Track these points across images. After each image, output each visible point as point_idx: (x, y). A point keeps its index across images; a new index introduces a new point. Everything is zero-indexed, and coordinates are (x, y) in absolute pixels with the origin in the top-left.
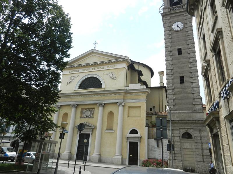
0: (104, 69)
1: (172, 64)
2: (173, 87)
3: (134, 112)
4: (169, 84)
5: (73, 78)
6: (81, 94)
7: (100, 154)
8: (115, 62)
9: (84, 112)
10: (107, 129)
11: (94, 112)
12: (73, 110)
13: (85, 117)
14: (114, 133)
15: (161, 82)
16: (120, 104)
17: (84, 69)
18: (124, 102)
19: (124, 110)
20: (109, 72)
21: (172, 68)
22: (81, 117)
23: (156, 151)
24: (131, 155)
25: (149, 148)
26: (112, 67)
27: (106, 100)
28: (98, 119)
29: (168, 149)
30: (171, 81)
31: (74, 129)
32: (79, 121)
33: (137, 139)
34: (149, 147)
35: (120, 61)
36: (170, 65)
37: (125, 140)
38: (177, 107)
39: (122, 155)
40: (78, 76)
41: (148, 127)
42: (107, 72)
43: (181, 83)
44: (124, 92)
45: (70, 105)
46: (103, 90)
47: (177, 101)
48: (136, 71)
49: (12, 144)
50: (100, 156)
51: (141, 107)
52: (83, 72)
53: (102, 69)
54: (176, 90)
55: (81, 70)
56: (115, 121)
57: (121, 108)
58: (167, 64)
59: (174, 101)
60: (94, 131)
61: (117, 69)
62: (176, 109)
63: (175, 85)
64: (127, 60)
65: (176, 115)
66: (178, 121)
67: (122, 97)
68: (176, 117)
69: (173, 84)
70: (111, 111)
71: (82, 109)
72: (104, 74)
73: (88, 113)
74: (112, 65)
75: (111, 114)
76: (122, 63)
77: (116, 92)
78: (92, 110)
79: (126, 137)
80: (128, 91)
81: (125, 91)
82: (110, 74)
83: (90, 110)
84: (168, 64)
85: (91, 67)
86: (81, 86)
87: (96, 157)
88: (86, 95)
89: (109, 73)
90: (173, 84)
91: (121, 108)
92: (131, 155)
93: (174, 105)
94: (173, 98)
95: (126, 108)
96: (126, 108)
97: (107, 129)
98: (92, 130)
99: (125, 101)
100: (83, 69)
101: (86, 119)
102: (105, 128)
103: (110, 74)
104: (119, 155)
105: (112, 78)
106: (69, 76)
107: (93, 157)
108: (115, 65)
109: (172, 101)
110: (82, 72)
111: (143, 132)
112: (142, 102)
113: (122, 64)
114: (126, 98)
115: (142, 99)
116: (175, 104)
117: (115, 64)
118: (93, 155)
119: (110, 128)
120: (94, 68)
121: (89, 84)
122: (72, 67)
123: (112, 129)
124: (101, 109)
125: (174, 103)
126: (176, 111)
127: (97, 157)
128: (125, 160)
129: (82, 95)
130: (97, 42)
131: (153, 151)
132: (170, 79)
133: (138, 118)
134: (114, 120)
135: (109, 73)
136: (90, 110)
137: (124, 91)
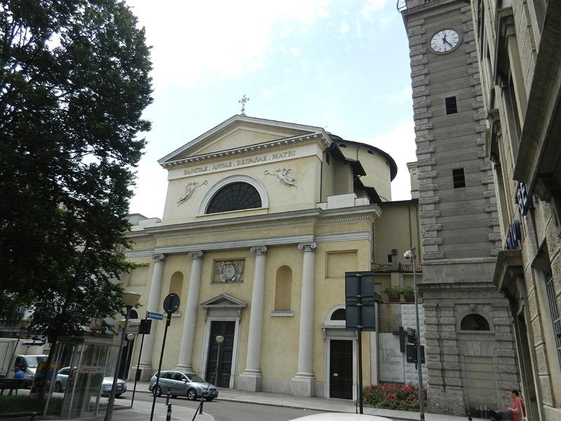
0: (265, 162)
1: (431, 138)
2: (437, 199)
5: (193, 187)
7: (260, 372)
10: (276, 310)
11: (243, 269)
12: (195, 263)
13: (224, 281)
15: (415, 189)
18: (315, 240)
19: (315, 263)
21: (431, 150)
22: (213, 282)
23: (397, 363)
24: (336, 375)
25: (381, 356)
26: (284, 155)
27: (271, 238)
31: (197, 310)
34: (381, 352)
35: (304, 139)
36: (428, 143)
37: (320, 336)
38: (446, 248)
40: (205, 183)
42: (272, 169)
46: (265, 212)
47: (446, 234)
51: (358, 252)
52: (217, 171)
53: (261, 163)
54: (443, 206)
55: (210, 168)
56: (294, 289)
59: (440, 233)
61: (297, 161)
64: (319, 136)
65: (445, 269)
67: (311, 229)
68: (444, 274)
69: (437, 190)
70: (290, 266)
71: (216, 261)
72: (267, 173)
73: (230, 272)
75: (285, 271)
76: (309, 144)
77: (296, 218)
80: (324, 214)
81: (318, 214)
90: (437, 190)
91: (308, 256)
92: (336, 375)
94: (436, 227)
95: (322, 257)
96: (322, 257)
97: (276, 310)
98: (240, 311)
102: (271, 306)
104: (252, 370)
105: (286, 184)
106: (185, 183)
107: (243, 378)
109: (435, 233)
110: (214, 171)
111: (62, 38)
113: (307, 147)
114: (319, 231)
115: (360, 232)
118: (242, 373)
119: (283, 307)
120: (241, 159)
122: (189, 161)
123: (287, 310)
124: (259, 260)
127: (253, 378)
128: (322, 387)
132: (428, 178)
134: (293, 285)
135: (278, 171)
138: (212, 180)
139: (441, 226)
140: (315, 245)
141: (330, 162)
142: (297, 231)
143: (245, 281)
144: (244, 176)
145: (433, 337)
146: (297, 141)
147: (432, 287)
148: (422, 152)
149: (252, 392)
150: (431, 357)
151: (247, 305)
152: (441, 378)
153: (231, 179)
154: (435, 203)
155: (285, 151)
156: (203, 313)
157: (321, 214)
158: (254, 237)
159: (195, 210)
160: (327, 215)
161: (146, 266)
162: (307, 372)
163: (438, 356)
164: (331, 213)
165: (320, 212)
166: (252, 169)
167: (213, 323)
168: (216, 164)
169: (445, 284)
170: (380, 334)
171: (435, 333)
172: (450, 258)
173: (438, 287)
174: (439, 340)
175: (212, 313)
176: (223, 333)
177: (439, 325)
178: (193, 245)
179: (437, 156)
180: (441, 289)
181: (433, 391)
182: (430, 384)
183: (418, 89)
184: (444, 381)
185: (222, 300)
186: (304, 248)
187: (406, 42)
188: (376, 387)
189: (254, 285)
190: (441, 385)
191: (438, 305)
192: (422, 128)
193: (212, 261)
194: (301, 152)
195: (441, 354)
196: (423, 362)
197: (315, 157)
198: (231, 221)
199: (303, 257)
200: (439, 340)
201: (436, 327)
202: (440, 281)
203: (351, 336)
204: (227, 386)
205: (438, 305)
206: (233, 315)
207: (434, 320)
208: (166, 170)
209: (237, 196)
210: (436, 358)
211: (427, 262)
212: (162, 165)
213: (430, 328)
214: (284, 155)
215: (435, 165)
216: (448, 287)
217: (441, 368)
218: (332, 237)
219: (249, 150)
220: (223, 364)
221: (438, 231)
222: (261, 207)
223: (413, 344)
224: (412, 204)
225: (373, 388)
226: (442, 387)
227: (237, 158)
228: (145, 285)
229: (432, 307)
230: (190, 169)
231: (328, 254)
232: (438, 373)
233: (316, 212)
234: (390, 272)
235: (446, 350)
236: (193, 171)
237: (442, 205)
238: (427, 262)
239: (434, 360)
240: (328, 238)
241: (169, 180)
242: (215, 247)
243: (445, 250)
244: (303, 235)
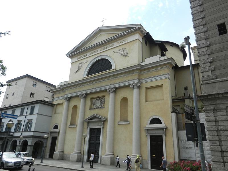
1: (201, 10)
2: (208, 43)
3: (154, 94)
4: (200, 40)
5: (81, 64)
7: (113, 154)
8: (125, 35)
10: (120, 121)
11: (104, 101)
12: (82, 100)
13: (95, 108)
14: (129, 125)
15: (196, 59)
16: (134, 85)
18: (139, 82)
19: (140, 94)
20: (119, 49)
21: (202, 16)
22: (91, 109)
23: (191, 148)
24: (154, 155)
25: (180, 144)
26: (122, 42)
28: (109, 109)
29: (190, 136)
30: (203, 35)
31: (83, 123)
32: (89, 114)
33: (161, 131)
34: (179, 141)
35: (132, 32)
36: (200, 13)
37: (144, 134)
38: (217, 72)
39: (141, 154)
41: (176, 112)
42: (116, 50)
43: (220, 35)
44: (138, 69)
46: (114, 70)
47: (216, 64)
48: (156, 45)
49: (23, 144)
50: (112, 157)
51: (163, 86)
52: (92, 55)
54: (213, 47)
55: (88, 54)
56: (129, 109)
57: (136, 91)
58: (194, 13)
59: (212, 64)
60: (106, 123)
61: (129, 44)
62: (216, 76)
63: (210, 40)
64: (139, 28)
65: (217, 85)
66: (222, 94)
67: (137, 77)
68: (217, 88)
69: (208, 39)
70: (124, 97)
71: (92, 99)
73: (98, 103)
75: (125, 100)
76: (134, 34)
77: (128, 71)
78: (102, 99)
79: (145, 129)
80: (143, 67)
81: (139, 67)
82: (120, 52)
83: (101, 99)
84: (196, 12)
85: (99, 48)
86: (90, 72)
87: (108, 158)
90: (208, 39)
91: (136, 91)
92: (154, 155)
93: (212, 71)
94: (209, 60)
95: (144, 91)
96: (144, 91)
97: (120, 121)
98: (102, 122)
99: (140, 81)
101: (97, 110)
102: (118, 119)
103: (120, 52)
104: (112, 154)
105: (123, 56)
106: (78, 63)
107: (104, 157)
108: (126, 39)
109: (208, 64)
110: (90, 55)
111: (169, 120)
112: (165, 79)
113: (133, 35)
114: (142, 77)
115: (163, 75)
116: (214, 68)
117: (125, 38)
118: (104, 155)
119: (124, 119)
120: (102, 48)
121: (98, 69)
123: (126, 120)
124: (112, 95)
125: (212, 68)
126: (217, 79)
127: (109, 158)
128: (146, 163)
129: (89, 82)
131: (187, 148)
132: (201, 33)
133: (160, 102)
134: (129, 107)
135: (119, 50)
136: (101, 99)
137: (137, 68)
139: (213, 59)
140: (139, 84)
141: (147, 45)
142: (129, 78)
144: (104, 55)
145: (212, 129)
146: (128, 33)
147: (209, 97)
148: (197, 18)
149: (108, 165)
150: (212, 143)
151: (106, 119)
152: (221, 157)
153: (98, 58)
154: (207, 47)
155: (122, 40)
156: (86, 124)
157: (142, 67)
159: (83, 74)
160: (145, 68)
161: (62, 104)
162: (110, 153)
163: (218, 142)
164: (146, 66)
165: (140, 66)
167: (91, 129)
168: (91, 52)
169: (218, 94)
170: (178, 131)
171: (214, 127)
172: (220, 78)
173: (213, 97)
174: (217, 131)
175: (90, 124)
176: (95, 136)
177: (216, 121)
178: (80, 91)
179: (206, 19)
180: (215, 98)
181: (216, 166)
182: (213, 162)
183: (197, 22)
184: (223, 159)
185: (94, 117)
186: (133, 87)
187: (195, 38)
188: (177, 163)
189: (109, 109)
190: (221, 162)
191: (214, 108)
192: (195, 6)
194: (130, 39)
195: (220, 141)
196: (204, 139)
197: (138, 40)
199: (133, 92)
200: (217, 131)
201: (214, 123)
202: (215, 93)
203: (162, 133)
204: (98, 162)
205: (214, 108)
206: (100, 125)
207: (213, 118)
208: (70, 59)
209: (101, 66)
210: (216, 143)
211: (204, 82)
212: (68, 56)
213: (210, 124)
214: (122, 42)
215: (205, 24)
216: (220, 96)
217: (220, 150)
218: (148, 79)
220: (96, 150)
221: (211, 63)
222: (112, 69)
223: (192, 122)
224: (196, 66)
225: (175, 163)
226: (223, 164)
227: (100, 47)
228: (61, 113)
229: (211, 110)
231: (147, 89)
232: (219, 154)
233: (138, 67)
234: (184, 99)
235: (223, 138)
236: (81, 57)
237: (211, 47)
238: (204, 82)
239: (215, 145)
240: (145, 80)
241: (71, 63)
242: (91, 91)
243: (216, 74)
244: (132, 79)
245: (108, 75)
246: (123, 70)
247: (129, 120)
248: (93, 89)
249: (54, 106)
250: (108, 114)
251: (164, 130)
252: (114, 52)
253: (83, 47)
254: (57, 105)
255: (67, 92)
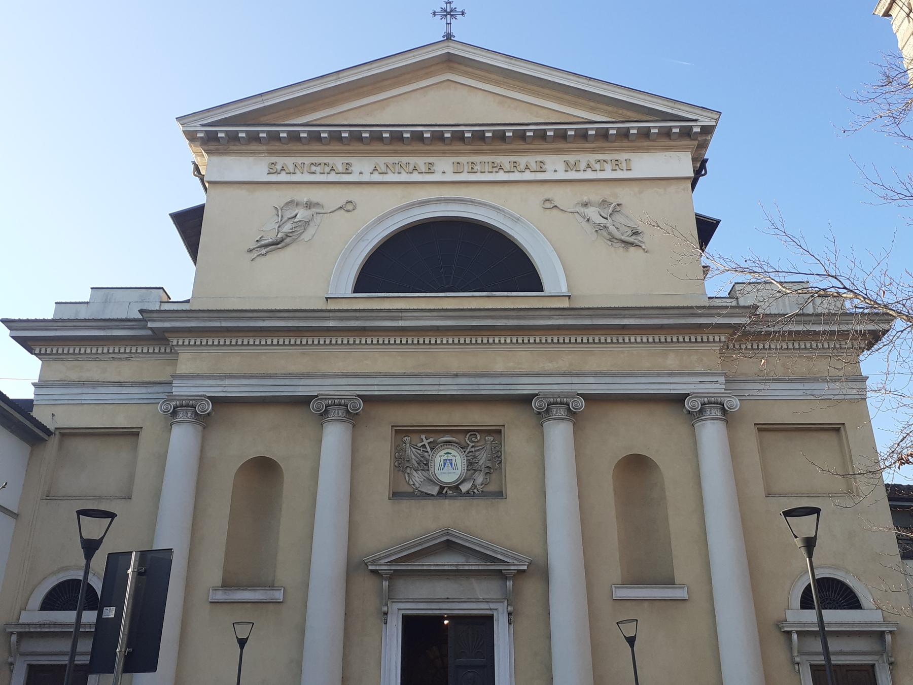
0: (540, 176)
5: (302, 214)
6: (401, 323)
8: (624, 134)
9: (412, 454)
11: (497, 458)
13: (435, 490)
17: (391, 160)
20: (585, 199)
27: (596, 375)
32: (403, 526)
35: (667, 133)
37: (779, 654)
40: (348, 207)
42: (564, 197)
45: (303, 402)
51: (143, 435)
53: (528, 176)
55: (363, 167)
71: (400, 432)
72: (550, 205)
74: (601, 157)
82: (592, 212)
88: (438, 330)
89: (585, 205)
91: (335, 436)
95: (749, 440)
97: (227, 585)
100: (381, 161)
102: (611, 569)
105: (612, 238)
106: (279, 197)
108: (623, 157)
110: (376, 177)
117: (620, 150)
122: (294, 137)
130: (457, 4)
135: (585, 205)
138: (380, 202)
142: (671, 361)
143: (511, 491)
158: (537, 368)
159: (323, 271)
166: (497, 189)
186: (174, 413)
193: (388, 431)
198: (219, 319)
214: (597, 166)
219: (418, 137)
227: (271, 153)
230: (289, 161)
245: (549, 317)
246: (184, 315)
247: (679, 577)
248: (427, 376)
249: (44, 440)
250: (231, 537)
251: (888, 638)
252: (548, 205)
253: (314, 110)
254: (67, 434)
255: (189, 361)
